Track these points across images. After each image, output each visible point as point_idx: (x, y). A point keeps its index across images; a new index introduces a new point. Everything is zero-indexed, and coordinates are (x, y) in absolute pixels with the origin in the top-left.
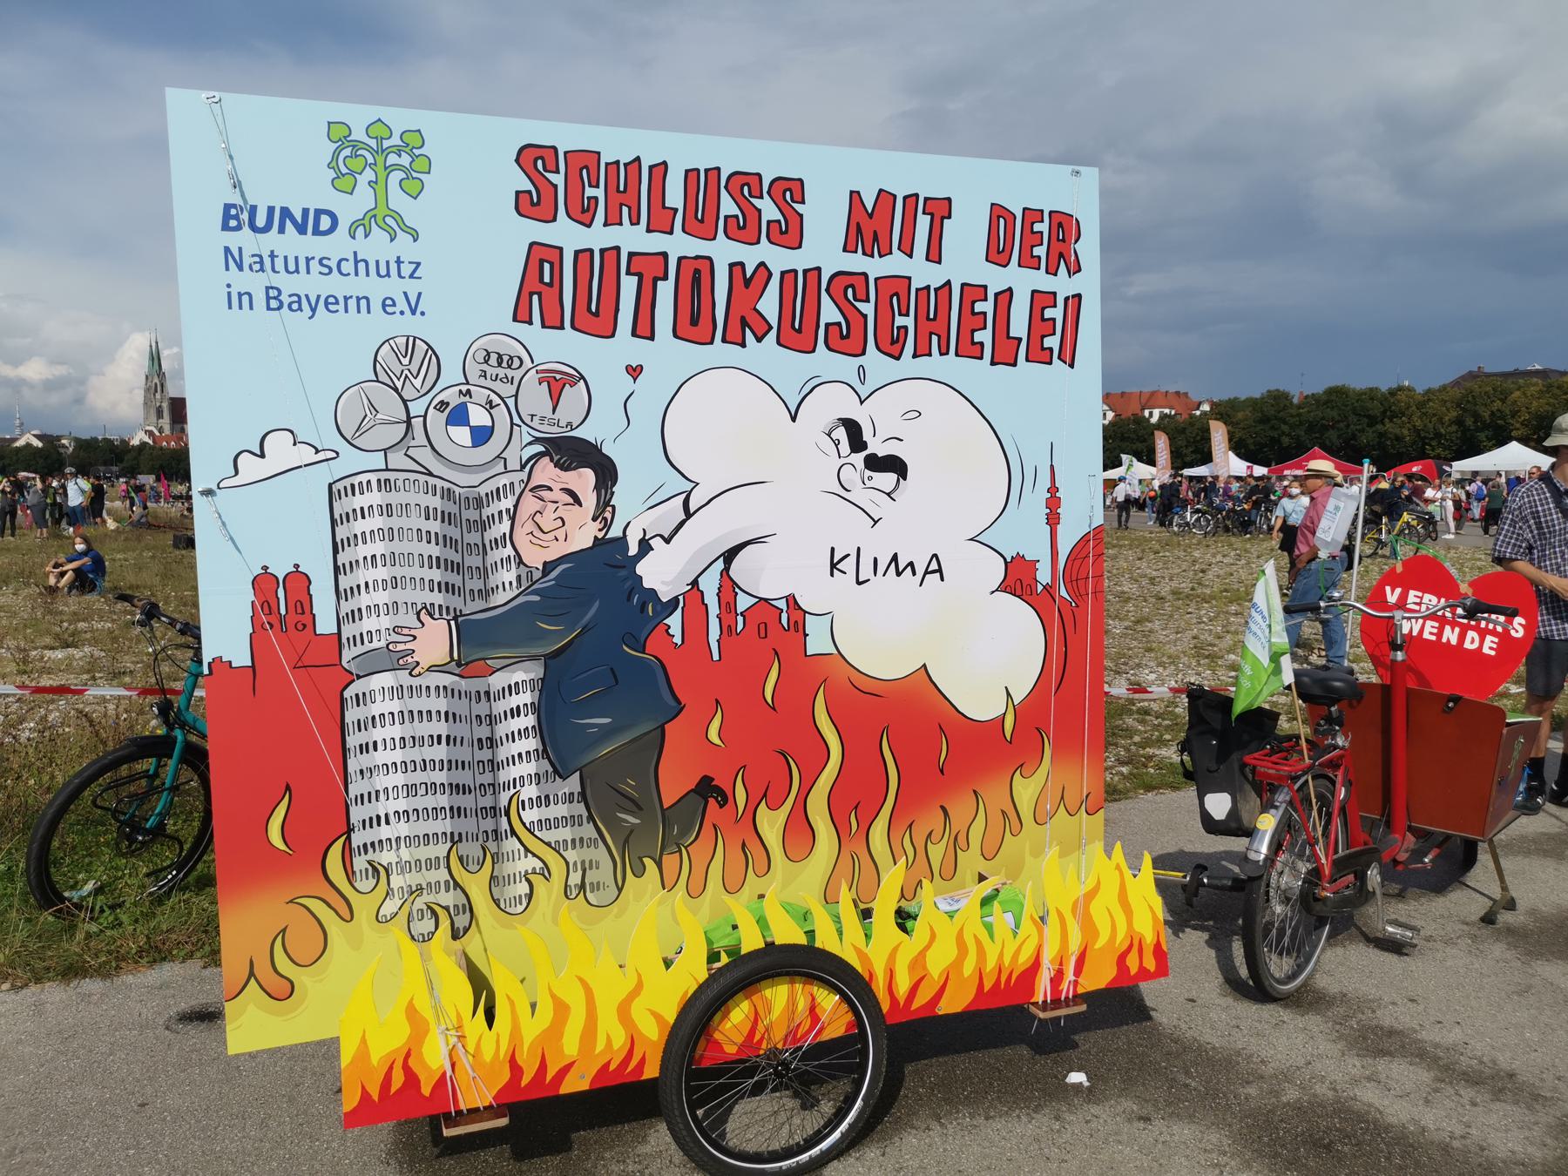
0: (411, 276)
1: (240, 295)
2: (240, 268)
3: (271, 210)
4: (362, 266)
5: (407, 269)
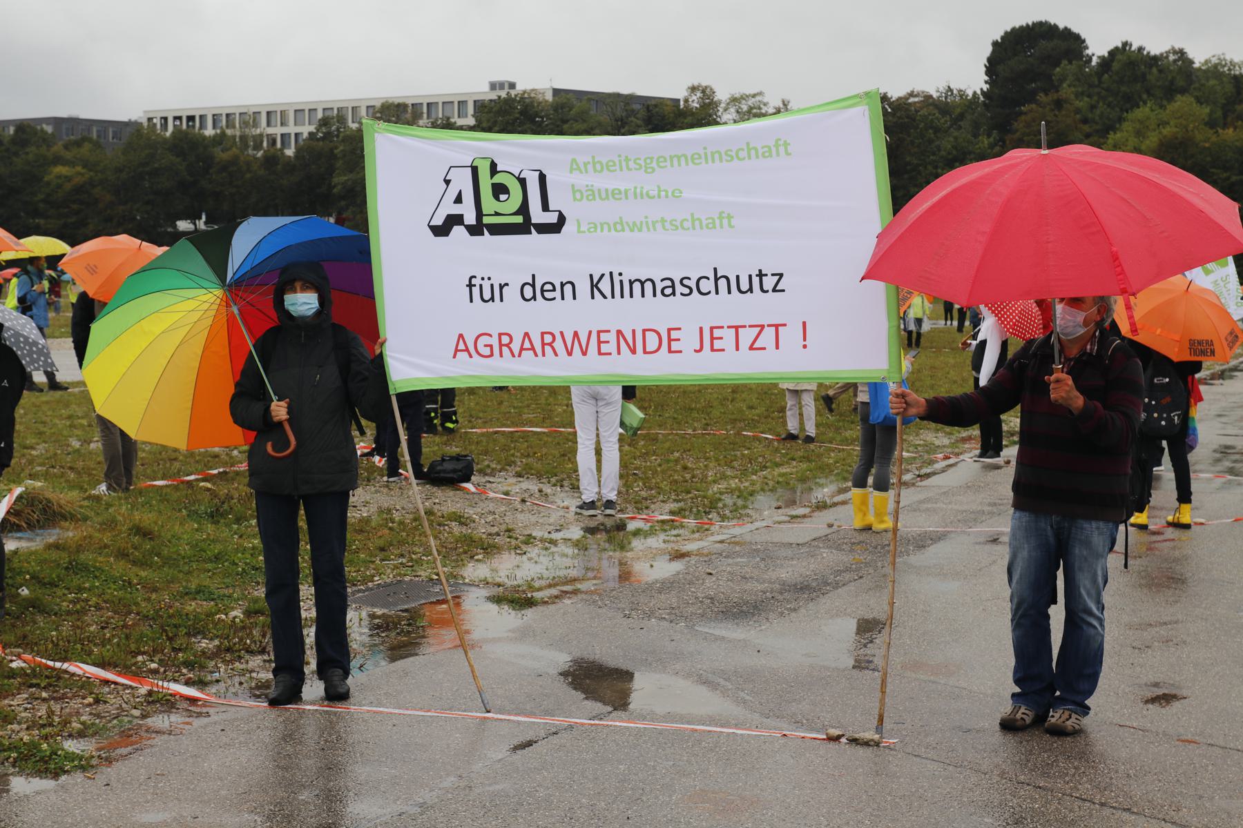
0: (774, 290)
1: (631, 283)
2: (619, 332)
3: (778, 155)
4: (722, 282)
5: (769, 282)
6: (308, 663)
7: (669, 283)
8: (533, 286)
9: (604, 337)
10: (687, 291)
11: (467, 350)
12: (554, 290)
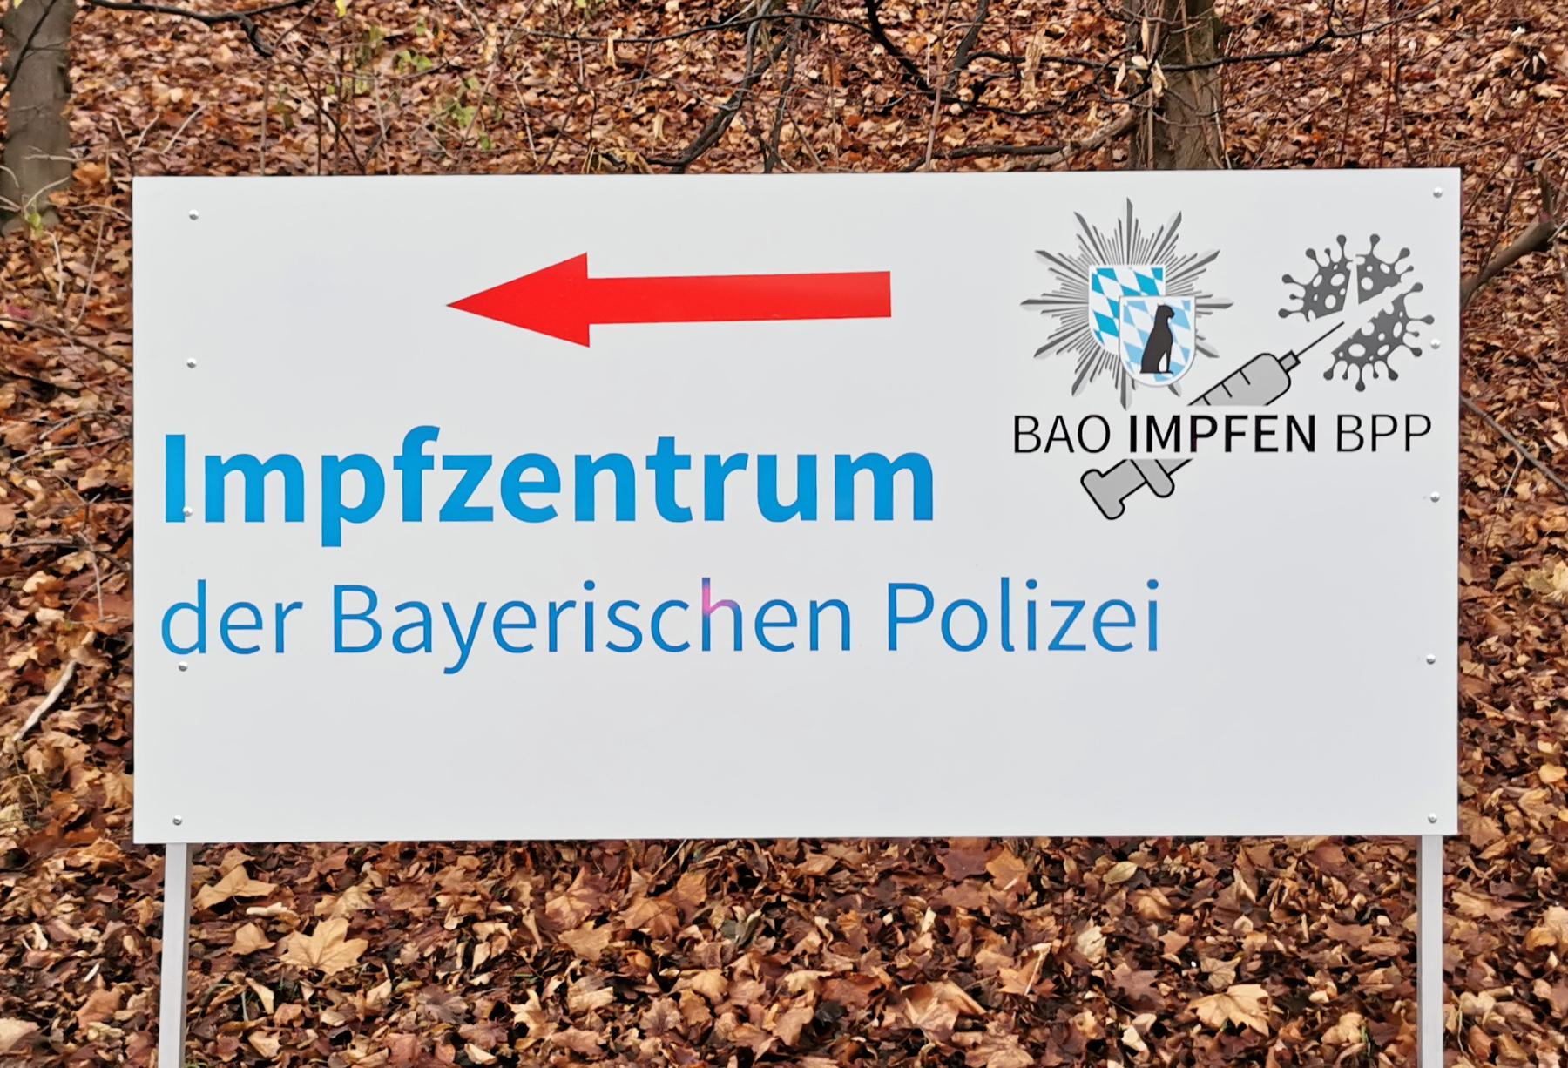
4: (722, 621)
6: (39, 584)
7: (416, 615)
8: (201, 610)
9: (1236, 426)
10: (627, 638)
11: (1067, 438)
12: (532, 624)
